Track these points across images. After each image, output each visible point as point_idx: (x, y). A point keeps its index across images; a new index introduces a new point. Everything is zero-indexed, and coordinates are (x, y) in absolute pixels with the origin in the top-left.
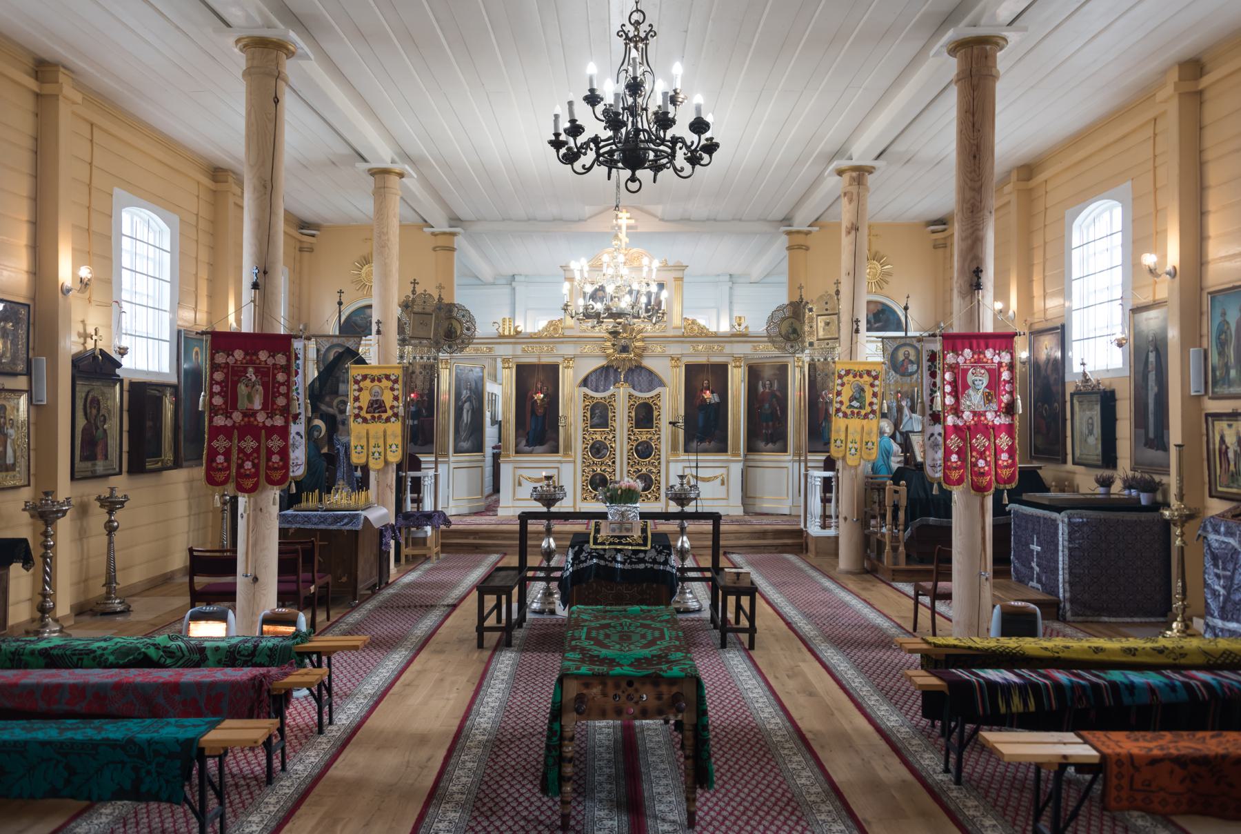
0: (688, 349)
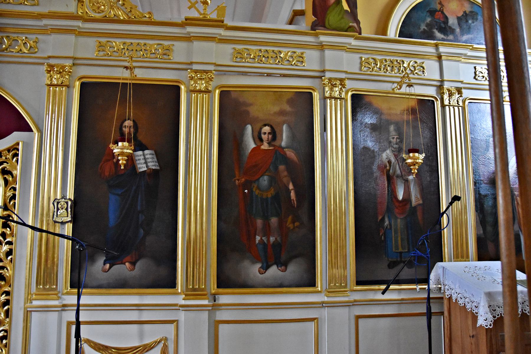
0: (88, 47)
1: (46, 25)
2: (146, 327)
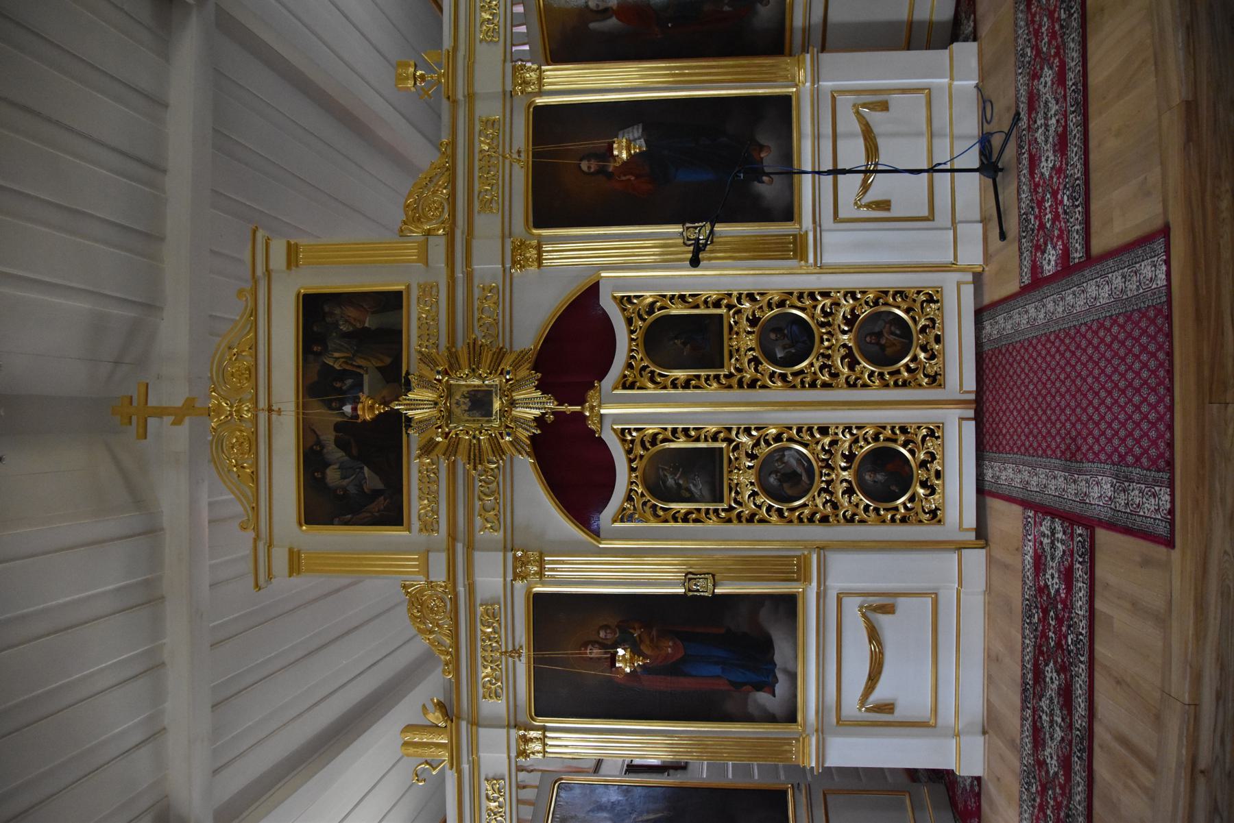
0: (487, 226)
2: (840, 129)
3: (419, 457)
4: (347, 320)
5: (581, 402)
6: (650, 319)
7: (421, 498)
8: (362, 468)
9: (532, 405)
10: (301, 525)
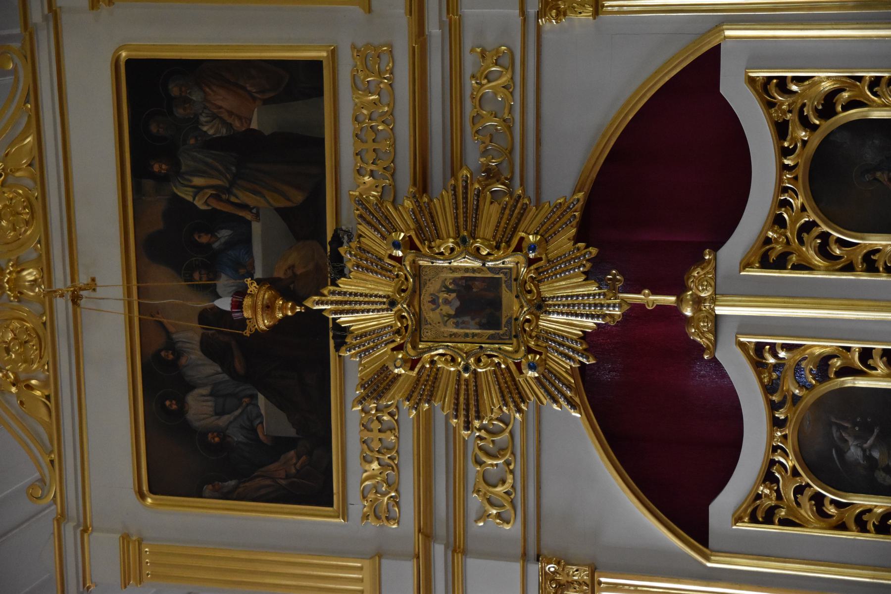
1: (462, 328)
3: (361, 400)
4: (221, 112)
5: (678, 287)
6: (827, 126)
7: (367, 460)
8: (253, 397)
9: (576, 309)
10: (142, 496)
